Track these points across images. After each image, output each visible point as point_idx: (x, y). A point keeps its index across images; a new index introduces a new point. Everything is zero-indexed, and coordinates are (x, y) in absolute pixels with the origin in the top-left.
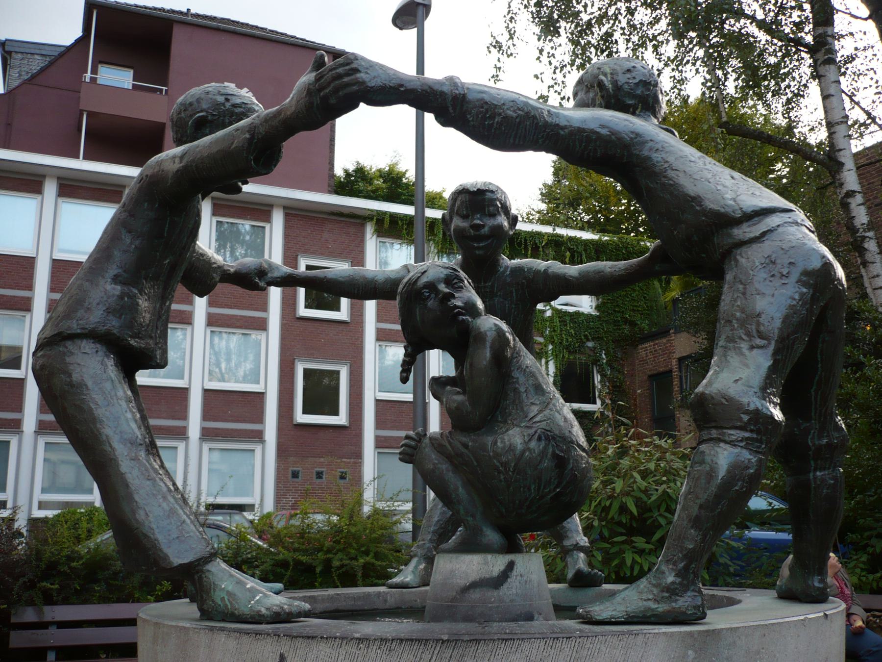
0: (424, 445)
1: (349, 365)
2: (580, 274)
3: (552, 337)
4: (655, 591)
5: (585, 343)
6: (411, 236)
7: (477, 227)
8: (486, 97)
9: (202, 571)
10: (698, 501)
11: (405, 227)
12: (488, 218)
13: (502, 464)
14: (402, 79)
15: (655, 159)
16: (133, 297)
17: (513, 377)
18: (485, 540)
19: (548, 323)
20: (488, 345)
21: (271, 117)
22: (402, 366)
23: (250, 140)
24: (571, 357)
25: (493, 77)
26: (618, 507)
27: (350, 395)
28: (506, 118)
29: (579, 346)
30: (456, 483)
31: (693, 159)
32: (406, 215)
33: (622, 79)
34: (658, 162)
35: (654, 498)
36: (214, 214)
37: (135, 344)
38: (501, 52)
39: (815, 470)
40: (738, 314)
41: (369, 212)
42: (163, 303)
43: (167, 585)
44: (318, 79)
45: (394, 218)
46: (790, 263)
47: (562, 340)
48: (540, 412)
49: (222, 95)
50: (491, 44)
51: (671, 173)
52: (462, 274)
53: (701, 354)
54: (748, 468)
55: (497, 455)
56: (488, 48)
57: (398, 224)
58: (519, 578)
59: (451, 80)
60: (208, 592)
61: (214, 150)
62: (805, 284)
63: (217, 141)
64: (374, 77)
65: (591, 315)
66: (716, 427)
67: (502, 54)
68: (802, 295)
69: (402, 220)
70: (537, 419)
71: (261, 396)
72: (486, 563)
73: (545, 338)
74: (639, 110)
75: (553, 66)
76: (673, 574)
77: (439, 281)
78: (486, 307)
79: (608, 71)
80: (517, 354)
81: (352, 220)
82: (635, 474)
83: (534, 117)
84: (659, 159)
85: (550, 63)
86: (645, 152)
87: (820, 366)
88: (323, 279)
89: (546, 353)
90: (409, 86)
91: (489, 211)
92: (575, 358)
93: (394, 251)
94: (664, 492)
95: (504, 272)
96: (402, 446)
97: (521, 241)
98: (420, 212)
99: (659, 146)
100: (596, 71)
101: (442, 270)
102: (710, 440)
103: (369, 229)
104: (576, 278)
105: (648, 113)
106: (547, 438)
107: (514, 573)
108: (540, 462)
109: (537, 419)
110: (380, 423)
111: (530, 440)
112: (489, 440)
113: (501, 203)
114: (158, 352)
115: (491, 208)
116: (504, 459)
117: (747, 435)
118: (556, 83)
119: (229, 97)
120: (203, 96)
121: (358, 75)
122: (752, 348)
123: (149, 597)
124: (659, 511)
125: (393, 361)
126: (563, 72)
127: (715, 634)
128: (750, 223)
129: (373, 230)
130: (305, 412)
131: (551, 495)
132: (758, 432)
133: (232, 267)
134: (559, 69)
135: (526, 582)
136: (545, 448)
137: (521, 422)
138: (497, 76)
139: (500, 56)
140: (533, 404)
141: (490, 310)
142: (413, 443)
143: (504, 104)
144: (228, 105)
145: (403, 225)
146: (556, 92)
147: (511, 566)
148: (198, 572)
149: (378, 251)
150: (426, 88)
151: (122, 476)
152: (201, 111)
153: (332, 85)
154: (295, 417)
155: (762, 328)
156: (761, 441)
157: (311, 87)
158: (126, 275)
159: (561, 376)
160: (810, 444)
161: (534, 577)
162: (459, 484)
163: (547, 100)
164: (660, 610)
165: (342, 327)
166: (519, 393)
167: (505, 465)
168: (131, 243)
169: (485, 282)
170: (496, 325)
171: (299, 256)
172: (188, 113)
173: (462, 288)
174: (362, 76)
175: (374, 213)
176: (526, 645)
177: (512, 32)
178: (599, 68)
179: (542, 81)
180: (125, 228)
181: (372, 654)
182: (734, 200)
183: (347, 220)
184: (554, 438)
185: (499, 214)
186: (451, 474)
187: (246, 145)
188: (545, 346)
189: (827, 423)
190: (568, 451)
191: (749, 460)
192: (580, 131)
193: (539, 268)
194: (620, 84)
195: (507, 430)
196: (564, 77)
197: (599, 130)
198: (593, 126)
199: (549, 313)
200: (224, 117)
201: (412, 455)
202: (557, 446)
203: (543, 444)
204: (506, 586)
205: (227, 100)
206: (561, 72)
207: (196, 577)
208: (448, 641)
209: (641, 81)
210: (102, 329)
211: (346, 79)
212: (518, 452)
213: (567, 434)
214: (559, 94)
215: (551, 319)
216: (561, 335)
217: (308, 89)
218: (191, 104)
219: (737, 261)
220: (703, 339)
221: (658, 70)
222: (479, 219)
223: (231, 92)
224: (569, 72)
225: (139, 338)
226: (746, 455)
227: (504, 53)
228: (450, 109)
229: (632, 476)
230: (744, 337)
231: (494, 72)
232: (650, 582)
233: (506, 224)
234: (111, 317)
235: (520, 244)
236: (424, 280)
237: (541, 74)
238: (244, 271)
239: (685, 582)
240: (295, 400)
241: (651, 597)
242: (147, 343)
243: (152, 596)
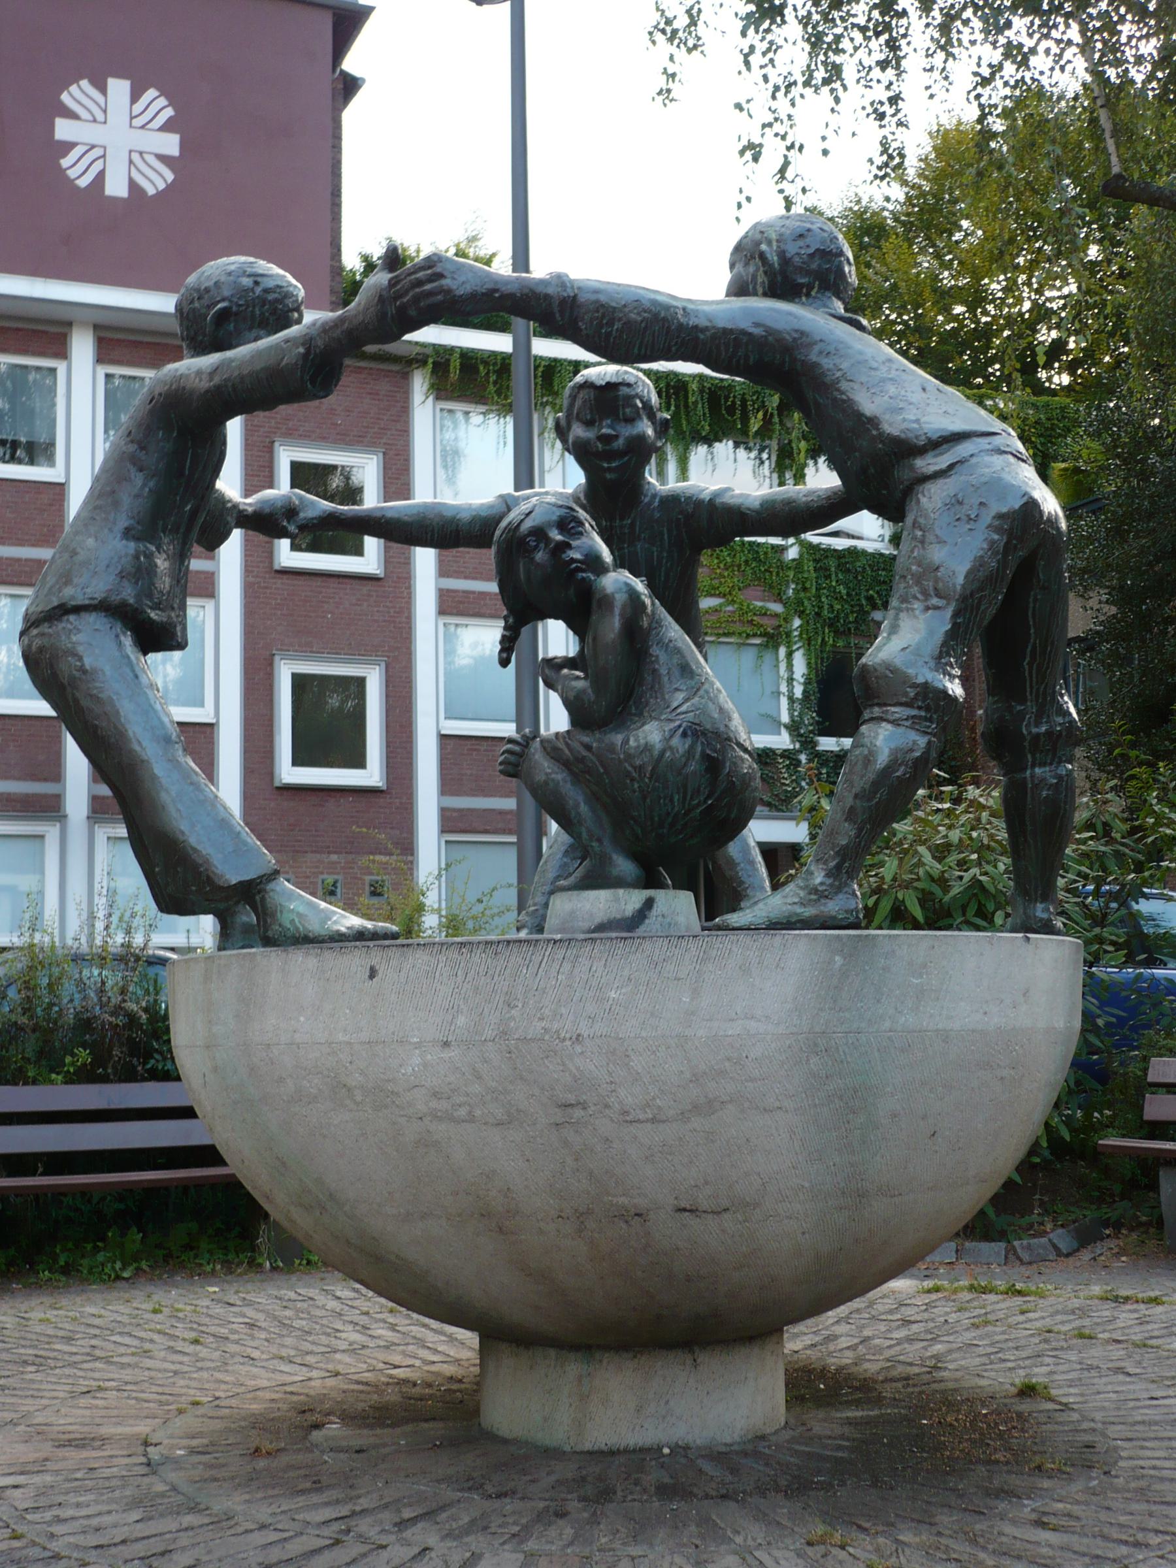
0: (532, 750)
1: (383, 665)
2: (761, 505)
3: (800, 602)
4: (802, 894)
5: (868, 613)
6: (506, 398)
7: (606, 439)
8: (603, 298)
9: (265, 890)
10: (854, 791)
11: (493, 378)
12: (623, 424)
13: (635, 768)
14: (496, 282)
15: (826, 366)
16: (149, 556)
17: (651, 655)
18: (615, 872)
19: (791, 574)
20: (617, 611)
21: (331, 328)
22: (501, 642)
23: (306, 356)
24: (840, 644)
25: (660, 93)
26: (889, 908)
27: (387, 726)
28: (628, 324)
29: (856, 621)
30: (576, 798)
31: (875, 365)
32: (494, 354)
33: (792, 249)
34: (829, 370)
35: (956, 890)
36: (100, 359)
37: (156, 618)
38: (676, 42)
39: (1033, 766)
40: (914, 568)
41: (418, 349)
42: (182, 562)
43: (84, 1056)
44: (392, 283)
45: (470, 360)
46: (981, 504)
47: (821, 608)
48: (686, 700)
49: (249, 276)
50: (655, 27)
51: (844, 385)
52: (582, 514)
53: (1097, 632)
54: (912, 750)
55: (629, 757)
56: (650, 33)
57: (477, 371)
58: (660, 919)
59: (560, 280)
60: (273, 915)
61: (258, 366)
62: (998, 530)
63: (259, 354)
64: (463, 283)
65: (882, 555)
66: (879, 705)
67: (678, 46)
68: (992, 543)
69: (486, 363)
70: (684, 708)
71: (208, 730)
72: (617, 900)
73: (785, 605)
74: (815, 290)
75: (770, 86)
76: (823, 874)
77: (550, 524)
78: (615, 559)
79: (774, 236)
80: (657, 623)
81: (382, 366)
82: (922, 849)
83: (665, 319)
84: (831, 366)
85: (766, 79)
86: (813, 357)
87: (1032, 631)
88: (380, 519)
89: (788, 635)
90: (505, 289)
91: (624, 413)
92: (848, 646)
93: (471, 428)
94: (975, 882)
95: (650, 503)
96: (503, 753)
97: (734, 402)
98: (523, 345)
99: (831, 349)
100: (758, 236)
101: (554, 509)
102: (872, 719)
103: (419, 384)
104: (757, 512)
105: (828, 294)
106: (695, 734)
108: (685, 765)
109: (684, 708)
110: (448, 783)
111: (671, 737)
112: (618, 738)
113: (642, 401)
114: (179, 628)
115: (628, 410)
116: (638, 762)
117: (914, 712)
118: (776, 119)
119: (259, 279)
120: (223, 279)
121: (444, 282)
122: (927, 608)
123: (54, 1076)
124: (964, 914)
125: (472, 657)
126: (790, 96)
128: (937, 451)
129: (426, 386)
130: (296, 762)
131: (701, 808)
132: (927, 709)
133: (250, 505)
134: (783, 90)
135: (670, 924)
136: (692, 747)
137: (661, 714)
138: (669, 91)
139: (673, 49)
140: (677, 690)
141: (621, 562)
142: (517, 748)
143: (625, 306)
144: (258, 290)
145: (488, 373)
146: (776, 135)
147: (649, 903)
148: (259, 892)
149: (438, 428)
150: (526, 291)
151: (154, 777)
152: (223, 300)
153: (411, 294)
154: (277, 772)
155: (940, 585)
156: (930, 720)
157: (384, 293)
158: (140, 528)
159: (818, 682)
160: (1025, 732)
161: (681, 919)
162: (581, 799)
163: (760, 153)
164: (807, 914)
165: (366, 588)
166: (660, 676)
167: (640, 769)
168: (144, 485)
169: (622, 519)
170: (627, 584)
171: (277, 444)
172: (205, 301)
173: (581, 534)
174: (446, 282)
175: (429, 351)
176: (647, 945)
177: (695, 12)
178: (762, 232)
179: (750, 116)
180: (134, 464)
181: (476, 959)
182: (917, 421)
183: (373, 365)
184: (704, 734)
185: (639, 417)
186: (569, 785)
187: (300, 363)
188: (786, 620)
189: (1048, 705)
190: (723, 751)
191: (914, 742)
192: (726, 332)
193: (702, 496)
194: (788, 255)
195: (643, 725)
196: (793, 105)
197: (751, 330)
198: (745, 325)
199: (793, 553)
200: (254, 307)
201: (516, 765)
202: (709, 744)
203: (689, 741)
205: (256, 283)
206: (786, 95)
207: (258, 898)
208: (561, 940)
209: (817, 250)
210: (115, 599)
211: (428, 287)
212: (656, 753)
213: (722, 729)
214: (784, 138)
215: (798, 564)
216: (818, 597)
217: (381, 296)
218: (207, 290)
219: (918, 501)
220: (1100, 602)
221: (990, 66)
222: (609, 427)
223: (261, 272)
224: (802, 96)
225: (160, 609)
226: (913, 736)
227: (682, 45)
228: (557, 315)
229: (916, 852)
230: (919, 596)
231: (661, 82)
232: (798, 886)
233: (650, 432)
234: (126, 583)
235: (731, 410)
236: (528, 524)
237: (748, 101)
238: (267, 510)
239: (837, 883)
240: (277, 738)
241: (796, 900)
242: (169, 617)
243: (58, 1074)
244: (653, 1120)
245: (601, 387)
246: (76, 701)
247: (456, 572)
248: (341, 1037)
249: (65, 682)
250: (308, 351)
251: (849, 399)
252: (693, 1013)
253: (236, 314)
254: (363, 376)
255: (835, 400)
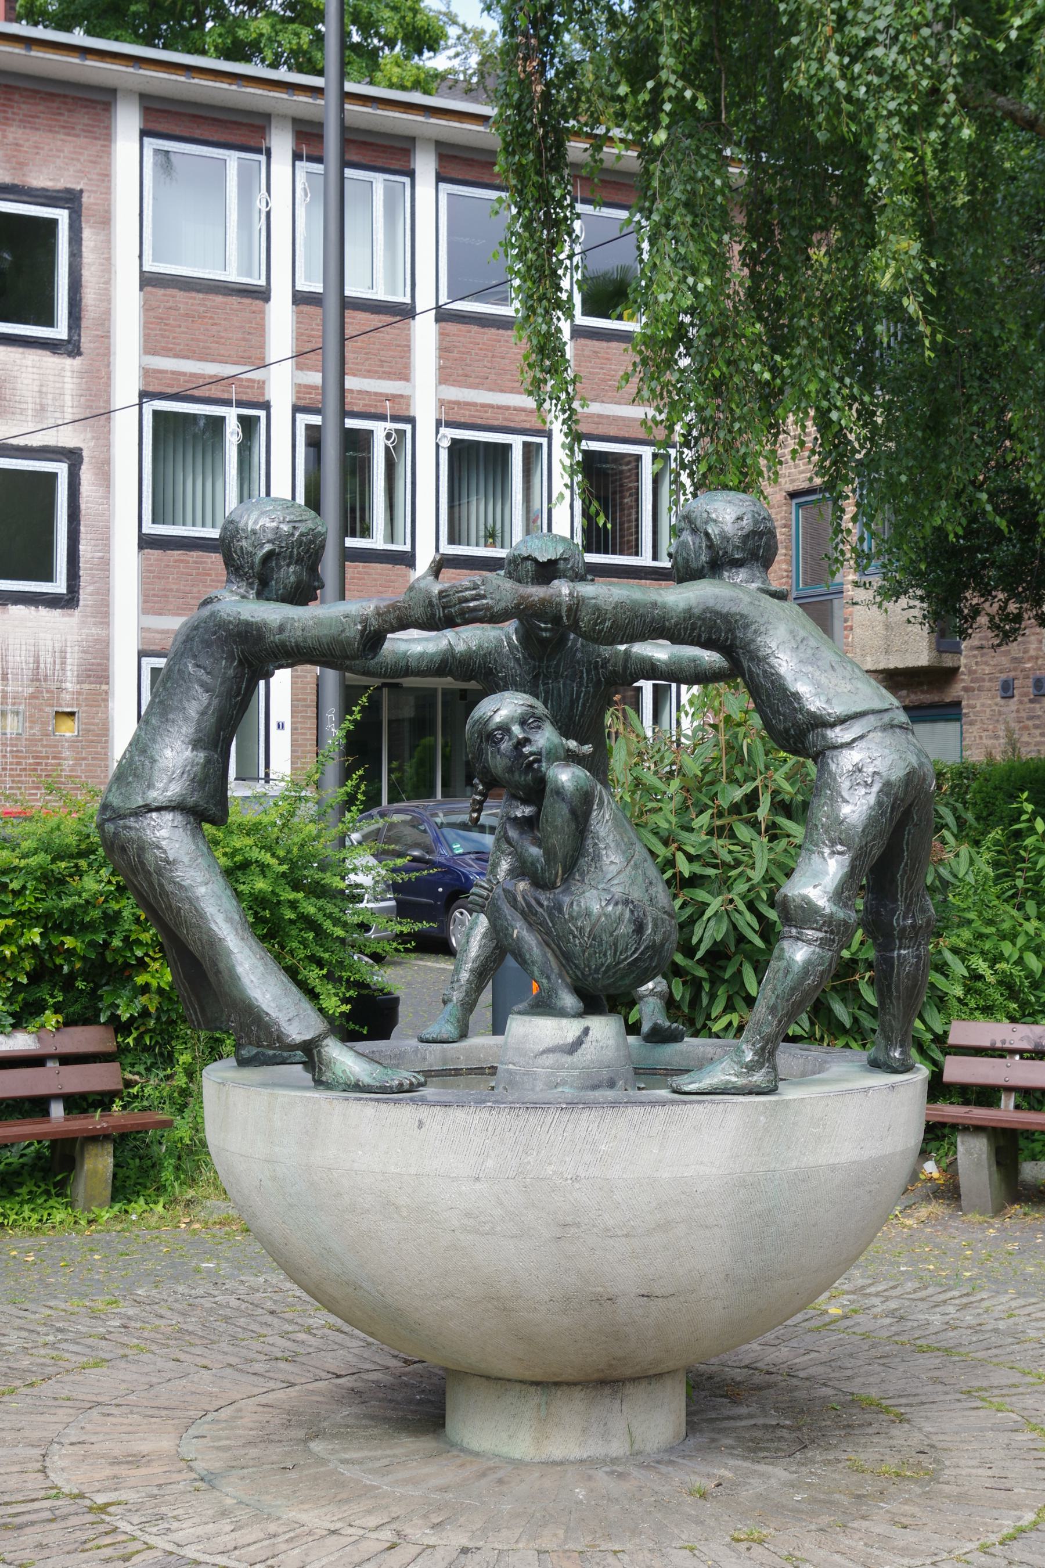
18: (559, 1004)
39: (900, 948)
86: (749, 635)
107: (589, 1038)
122: (833, 853)
127: (787, 1103)
147: (586, 1031)
204: (580, 1051)
244: (626, 1236)
245: (544, 563)
246: (161, 885)
247: (164, 349)
248: (393, 1169)
249: (152, 870)
250: (365, 628)
251: (777, 674)
252: (660, 1161)
253: (279, 554)
254: (55, 105)
255: (765, 672)
